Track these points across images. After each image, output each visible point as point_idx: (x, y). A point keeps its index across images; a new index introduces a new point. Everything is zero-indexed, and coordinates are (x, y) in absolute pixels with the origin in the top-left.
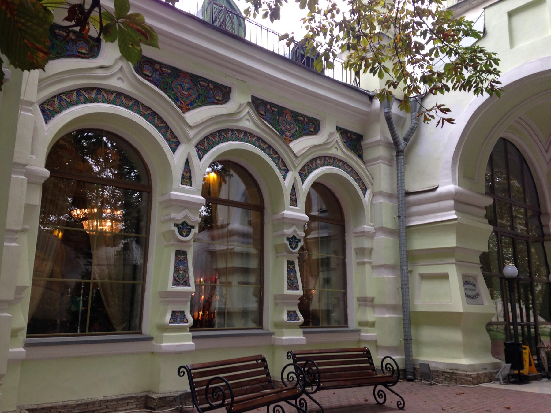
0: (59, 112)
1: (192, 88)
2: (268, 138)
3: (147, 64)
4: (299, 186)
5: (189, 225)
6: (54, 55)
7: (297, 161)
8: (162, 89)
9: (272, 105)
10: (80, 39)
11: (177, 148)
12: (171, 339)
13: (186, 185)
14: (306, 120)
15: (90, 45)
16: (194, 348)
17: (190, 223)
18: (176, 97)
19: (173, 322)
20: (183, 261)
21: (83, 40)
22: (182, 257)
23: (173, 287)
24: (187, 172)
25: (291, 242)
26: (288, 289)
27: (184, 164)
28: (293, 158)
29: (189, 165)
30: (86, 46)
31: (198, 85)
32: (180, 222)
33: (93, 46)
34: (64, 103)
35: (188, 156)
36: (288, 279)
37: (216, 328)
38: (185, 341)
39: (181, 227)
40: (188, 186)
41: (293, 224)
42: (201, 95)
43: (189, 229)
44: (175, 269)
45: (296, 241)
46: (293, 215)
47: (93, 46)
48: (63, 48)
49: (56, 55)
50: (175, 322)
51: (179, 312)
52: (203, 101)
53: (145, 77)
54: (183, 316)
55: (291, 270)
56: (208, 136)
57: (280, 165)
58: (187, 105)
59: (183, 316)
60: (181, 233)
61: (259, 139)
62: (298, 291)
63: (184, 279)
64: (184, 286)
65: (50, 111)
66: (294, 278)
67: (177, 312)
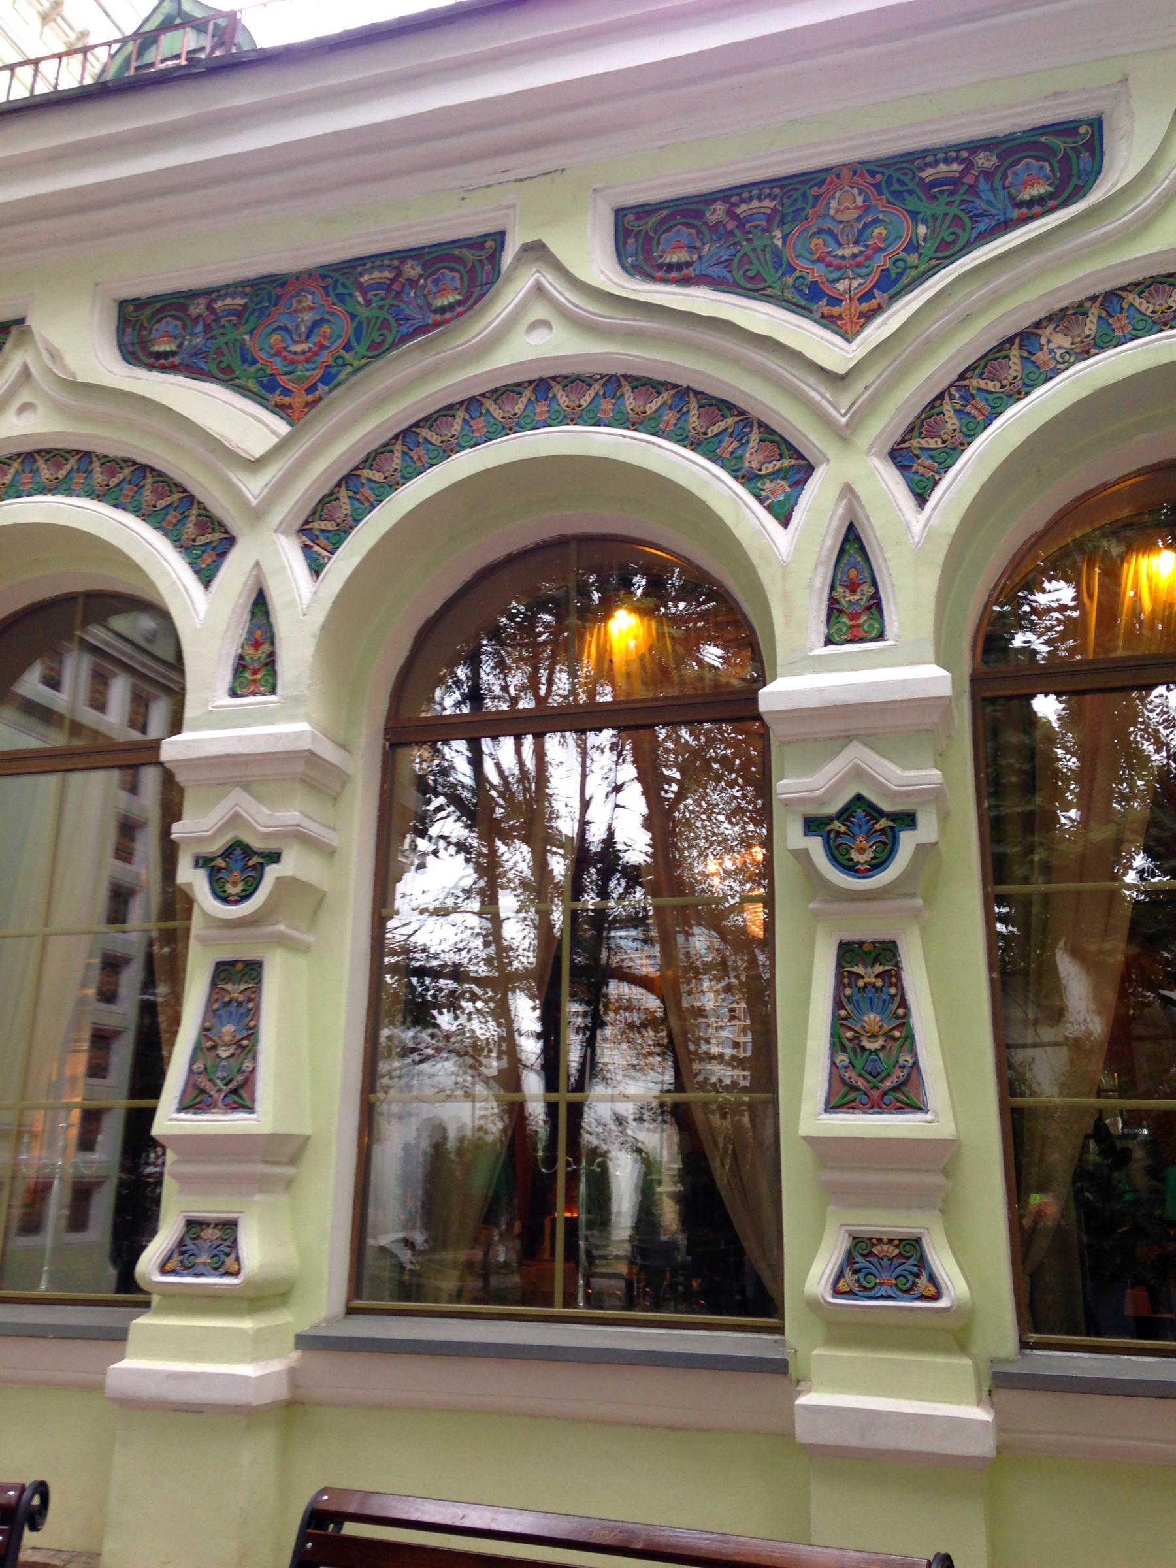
0: (962, 444)
1: (327, 317)
2: (657, 357)
3: (162, 319)
4: (876, 527)
5: (255, 853)
6: (932, 259)
7: (845, 401)
8: (220, 375)
9: (730, 195)
10: (1017, 156)
11: (221, 563)
12: (159, 1345)
13: (254, 693)
14: (412, 270)
15: (469, 267)
16: (985, 1447)
17: (257, 844)
18: (265, 379)
19: (856, 1289)
20: (240, 1004)
21: (441, 265)
22: (869, 974)
23: (183, 1116)
24: (257, 645)
25: (844, 840)
26: (832, 1106)
27: (247, 616)
28: (818, 393)
29: (267, 613)
30: (1027, 166)
31: (351, 295)
32: (215, 847)
33: (1072, 154)
34: (173, 517)
35: (850, 509)
36: (837, 1044)
37: (43, 1288)
38: (232, 1360)
39: (843, 829)
40: (263, 694)
41: (847, 738)
42: (369, 322)
43: (883, 831)
44: (203, 1040)
45: (883, 823)
46: (820, 691)
47: (1072, 154)
48: (961, 219)
49: (940, 255)
50: (188, 1268)
51: (216, 1225)
52: (374, 346)
53: (157, 364)
54: (912, 1261)
55: (870, 992)
56: (357, 468)
57: (752, 458)
58: (311, 389)
59: (912, 1261)
60: (841, 859)
61: (613, 383)
62: (920, 1116)
63: (231, 1080)
64: (225, 1113)
65: (932, 453)
66: (888, 1036)
67: (208, 1225)
